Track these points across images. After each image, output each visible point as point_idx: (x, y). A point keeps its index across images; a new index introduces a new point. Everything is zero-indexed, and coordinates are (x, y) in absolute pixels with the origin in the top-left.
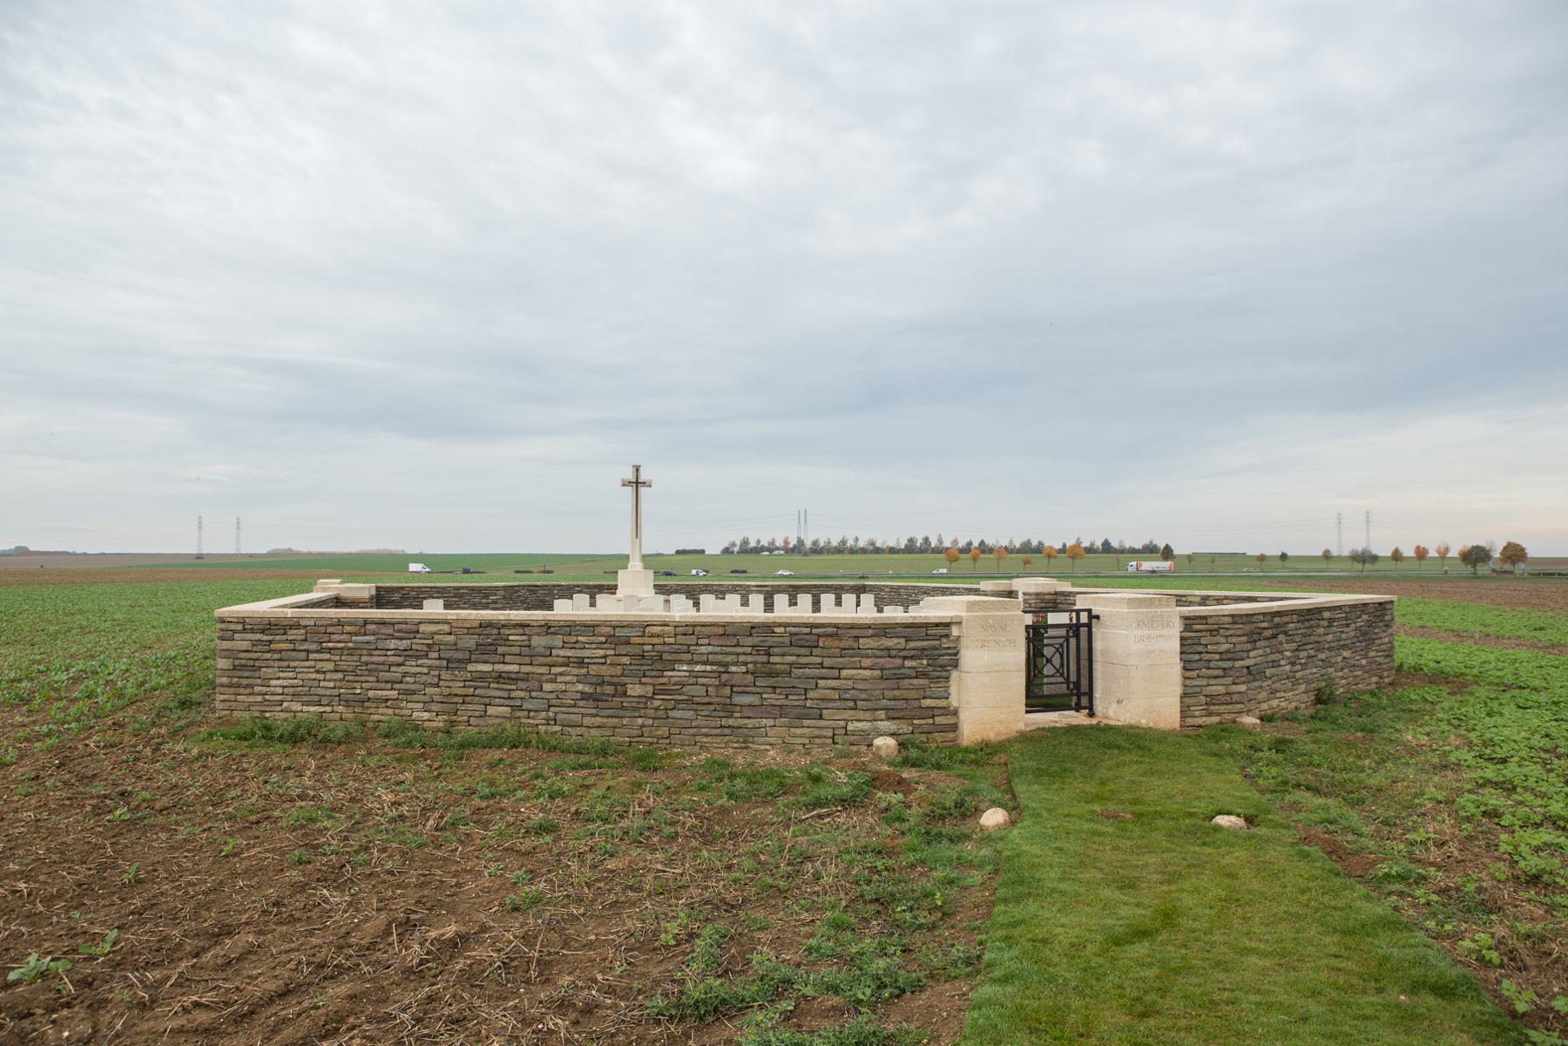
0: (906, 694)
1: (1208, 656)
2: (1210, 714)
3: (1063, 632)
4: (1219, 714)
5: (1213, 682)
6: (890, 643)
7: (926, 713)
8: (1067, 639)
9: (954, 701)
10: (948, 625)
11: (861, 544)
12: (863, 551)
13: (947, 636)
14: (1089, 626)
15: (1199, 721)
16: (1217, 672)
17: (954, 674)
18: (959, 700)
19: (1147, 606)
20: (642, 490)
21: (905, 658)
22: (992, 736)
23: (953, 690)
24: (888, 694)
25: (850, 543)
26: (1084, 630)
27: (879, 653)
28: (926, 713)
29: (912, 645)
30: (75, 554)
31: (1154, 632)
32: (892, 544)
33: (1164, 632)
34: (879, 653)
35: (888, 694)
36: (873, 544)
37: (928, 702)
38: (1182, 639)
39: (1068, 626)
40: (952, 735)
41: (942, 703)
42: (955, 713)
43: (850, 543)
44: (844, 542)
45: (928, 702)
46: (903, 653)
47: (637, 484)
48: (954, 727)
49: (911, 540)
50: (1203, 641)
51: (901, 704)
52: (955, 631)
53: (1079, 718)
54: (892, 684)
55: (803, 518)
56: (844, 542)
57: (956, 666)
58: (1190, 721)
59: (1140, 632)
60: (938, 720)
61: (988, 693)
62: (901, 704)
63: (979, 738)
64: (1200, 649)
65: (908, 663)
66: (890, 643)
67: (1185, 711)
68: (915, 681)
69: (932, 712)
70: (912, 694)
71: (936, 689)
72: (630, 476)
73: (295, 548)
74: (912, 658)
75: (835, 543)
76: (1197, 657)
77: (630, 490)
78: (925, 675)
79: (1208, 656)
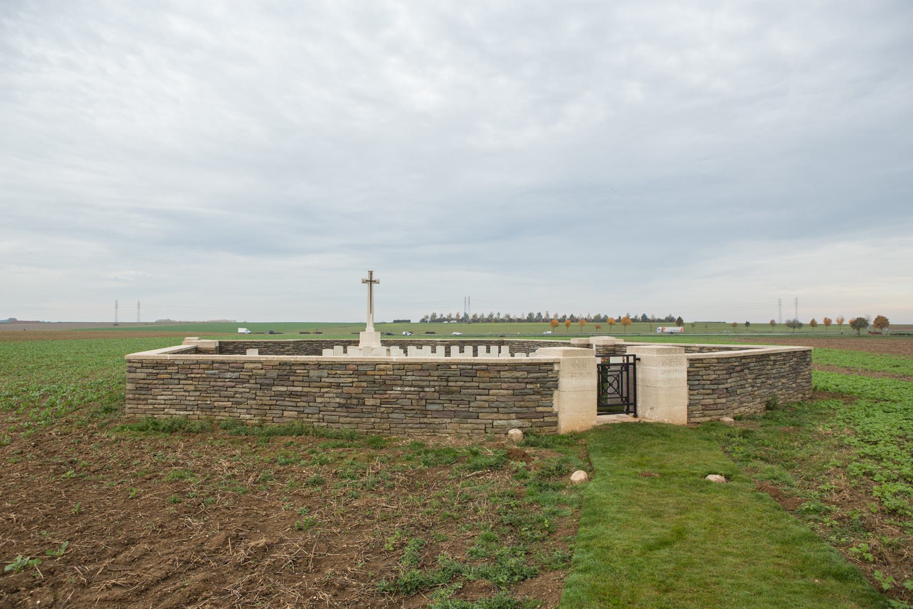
0: (527, 404)
1: (704, 382)
2: (705, 416)
3: (619, 368)
4: (710, 416)
5: (706, 397)
6: (518, 374)
7: (539, 415)
8: (621, 372)
9: (555, 408)
10: (552, 364)
11: (502, 317)
12: (503, 321)
13: (551, 370)
14: (634, 364)
15: (698, 420)
16: (708, 391)
17: (556, 393)
18: (558, 408)
19: (668, 353)
20: (374, 285)
21: (527, 383)
22: (578, 429)
23: (555, 402)
24: (517, 404)
25: (495, 316)
26: (631, 367)
27: (512, 380)
28: (539, 415)
29: (531, 375)
30: (43, 323)
31: (672, 368)
32: (520, 317)
33: (678, 368)
34: (512, 380)
35: (517, 404)
36: (508, 317)
37: (540, 409)
38: (688, 372)
39: (622, 365)
40: (554, 428)
41: (549, 409)
42: (556, 415)
43: (495, 316)
44: (491, 316)
45: (540, 409)
46: (526, 380)
47: (371, 282)
48: (556, 423)
49: (530, 315)
50: (701, 373)
51: (525, 410)
52: (556, 368)
53: (628, 418)
54: (519, 398)
55: (467, 301)
56: (491, 316)
57: (557, 388)
58: (693, 420)
59: (664, 368)
60: (546, 419)
61: (575, 404)
62: (525, 410)
63: (570, 430)
64: (699, 378)
65: (529, 386)
66: (518, 374)
67: (690, 414)
68: (533, 397)
69: (542, 415)
70: (531, 404)
71: (545, 401)
72: (367, 277)
73: (172, 319)
74: (531, 383)
75: (486, 316)
76: (697, 382)
77: (367, 285)
78: (538, 393)
79: (704, 382)
